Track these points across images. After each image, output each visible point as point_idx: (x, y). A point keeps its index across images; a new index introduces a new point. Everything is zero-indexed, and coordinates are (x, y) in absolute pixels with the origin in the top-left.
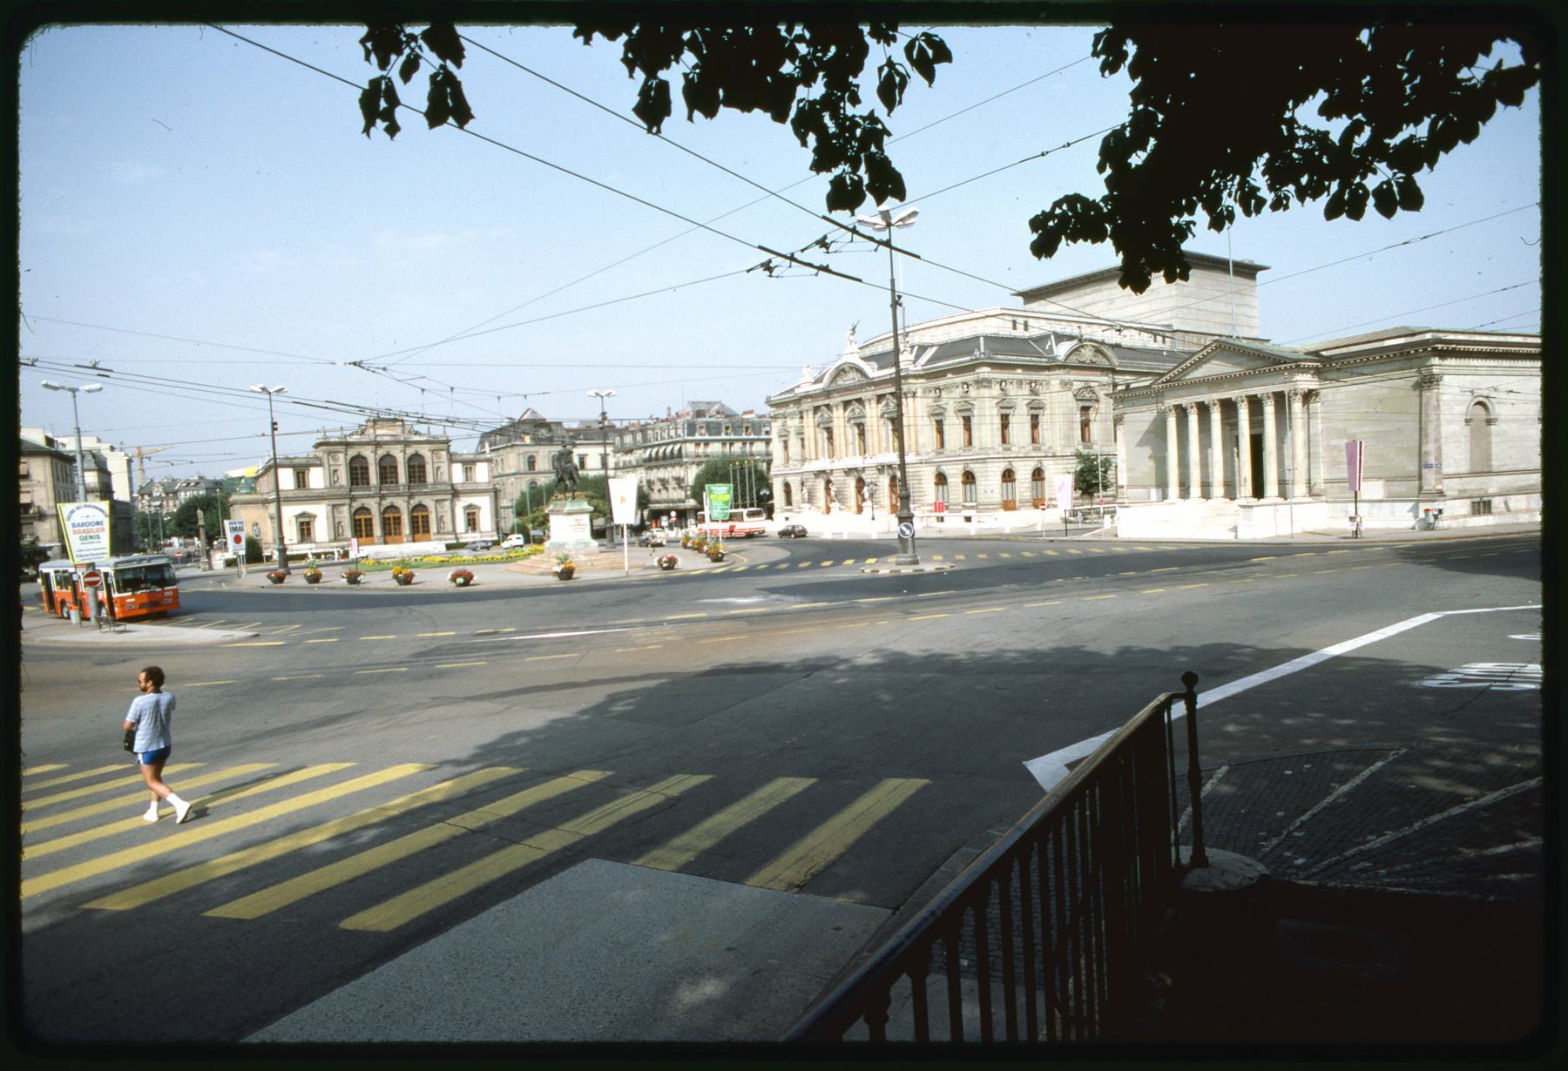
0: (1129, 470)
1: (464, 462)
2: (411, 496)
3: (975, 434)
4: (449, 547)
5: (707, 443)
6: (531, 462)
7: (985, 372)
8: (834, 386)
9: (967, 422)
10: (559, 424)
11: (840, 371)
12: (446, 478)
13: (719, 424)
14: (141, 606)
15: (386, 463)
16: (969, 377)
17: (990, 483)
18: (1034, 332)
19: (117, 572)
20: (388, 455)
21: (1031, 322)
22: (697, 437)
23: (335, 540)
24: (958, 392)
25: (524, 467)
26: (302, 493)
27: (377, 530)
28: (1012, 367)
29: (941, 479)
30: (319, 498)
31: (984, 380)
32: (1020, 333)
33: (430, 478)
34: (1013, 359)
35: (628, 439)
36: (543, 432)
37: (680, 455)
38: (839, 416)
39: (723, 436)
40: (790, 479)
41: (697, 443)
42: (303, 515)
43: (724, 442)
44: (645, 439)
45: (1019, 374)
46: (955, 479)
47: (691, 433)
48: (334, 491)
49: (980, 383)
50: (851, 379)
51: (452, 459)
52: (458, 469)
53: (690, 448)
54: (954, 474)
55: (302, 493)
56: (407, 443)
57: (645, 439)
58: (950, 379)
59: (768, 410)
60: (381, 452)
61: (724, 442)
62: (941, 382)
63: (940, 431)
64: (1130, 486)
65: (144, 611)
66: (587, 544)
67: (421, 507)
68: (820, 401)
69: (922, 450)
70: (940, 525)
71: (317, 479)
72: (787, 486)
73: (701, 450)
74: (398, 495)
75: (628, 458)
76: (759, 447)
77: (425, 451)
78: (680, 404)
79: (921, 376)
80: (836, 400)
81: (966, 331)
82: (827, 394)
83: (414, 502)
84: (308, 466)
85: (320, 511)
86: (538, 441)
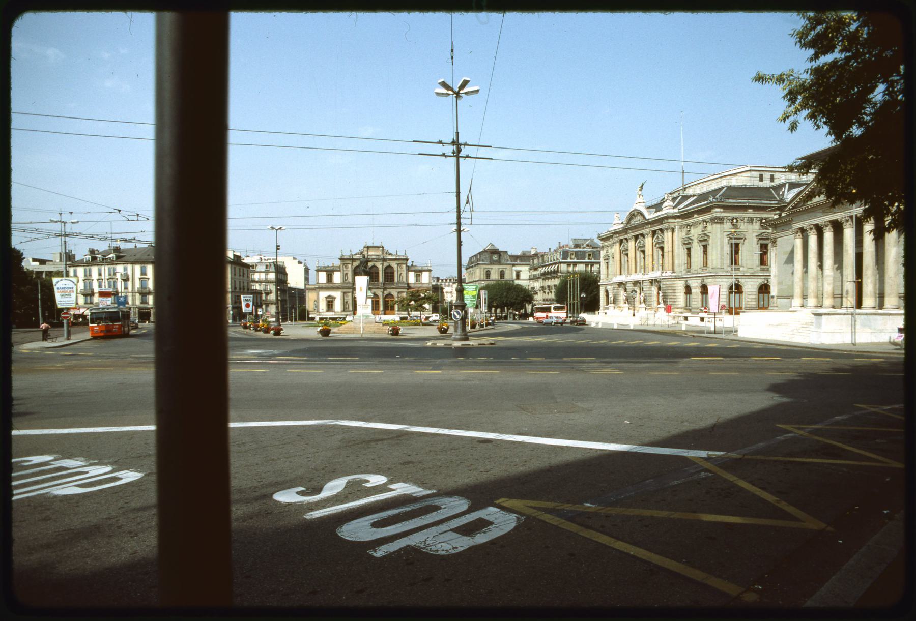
0: (780, 283)
1: (416, 271)
2: (385, 289)
3: (709, 258)
4: (402, 319)
5: (575, 264)
6: (488, 274)
7: (717, 212)
8: (629, 226)
9: (705, 247)
10: (506, 252)
11: (632, 216)
12: (404, 280)
13: (584, 252)
14: (101, 331)
15: (389, 271)
16: (707, 217)
17: (718, 291)
18: (777, 182)
19: (92, 314)
20: (374, 266)
21: (777, 175)
22: (569, 260)
23: (344, 311)
24: (700, 228)
25: (483, 277)
26: (330, 285)
27: (381, 308)
28: (744, 208)
29: (688, 290)
30: (337, 288)
31: (716, 218)
32: (767, 183)
33: (396, 280)
34: (745, 202)
35: (536, 261)
36: (495, 258)
37: (557, 272)
38: (631, 244)
39: (587, 260)
40: (609, 288)
41: (569, 264)
42: (329, 297)
43: (587, 264)
44: (543, 262)
45: (750, 214)
46: (696, 291)
47: (565, 257)
48: (345, 285)
49: (714, 220)
50: (638, 220)
51: (409, 269)
52: (412, 275)
53: (564, 267)
54: (695, 284)
55: (330, 285)
56: (384, 260)
57: (543, 262)
58: (697, 218)
59: (600, 243)
60: (386, 264)
61: (587, 264)
62: (691, 221)
63: (689, 255)
64: (779, 297)
65: (102, 334)
66: (367, 317)
67: (390, 295)
68: (620, 236)
69: (676, 269)
70: (702, 324)
71: (337, 278)
72: (607, 291)
73: (571, 269)
74: (378, 288)
75: (536, 273)
76: (595, 268)
77: (394, 265)
78: (567, 241)
79: (678, 217)
80: (631, 234)
81: (714, 186)
82: (625, 231)
83: (386, 293)
84: (333, 271)
85: (338, 295)
86: (492, 263)
